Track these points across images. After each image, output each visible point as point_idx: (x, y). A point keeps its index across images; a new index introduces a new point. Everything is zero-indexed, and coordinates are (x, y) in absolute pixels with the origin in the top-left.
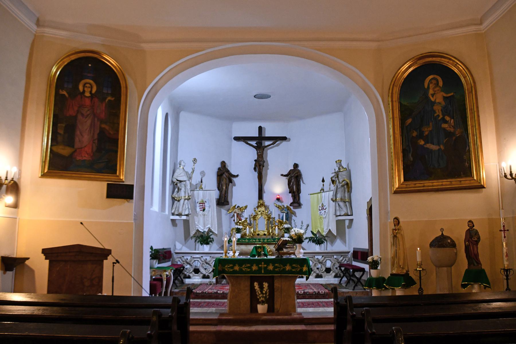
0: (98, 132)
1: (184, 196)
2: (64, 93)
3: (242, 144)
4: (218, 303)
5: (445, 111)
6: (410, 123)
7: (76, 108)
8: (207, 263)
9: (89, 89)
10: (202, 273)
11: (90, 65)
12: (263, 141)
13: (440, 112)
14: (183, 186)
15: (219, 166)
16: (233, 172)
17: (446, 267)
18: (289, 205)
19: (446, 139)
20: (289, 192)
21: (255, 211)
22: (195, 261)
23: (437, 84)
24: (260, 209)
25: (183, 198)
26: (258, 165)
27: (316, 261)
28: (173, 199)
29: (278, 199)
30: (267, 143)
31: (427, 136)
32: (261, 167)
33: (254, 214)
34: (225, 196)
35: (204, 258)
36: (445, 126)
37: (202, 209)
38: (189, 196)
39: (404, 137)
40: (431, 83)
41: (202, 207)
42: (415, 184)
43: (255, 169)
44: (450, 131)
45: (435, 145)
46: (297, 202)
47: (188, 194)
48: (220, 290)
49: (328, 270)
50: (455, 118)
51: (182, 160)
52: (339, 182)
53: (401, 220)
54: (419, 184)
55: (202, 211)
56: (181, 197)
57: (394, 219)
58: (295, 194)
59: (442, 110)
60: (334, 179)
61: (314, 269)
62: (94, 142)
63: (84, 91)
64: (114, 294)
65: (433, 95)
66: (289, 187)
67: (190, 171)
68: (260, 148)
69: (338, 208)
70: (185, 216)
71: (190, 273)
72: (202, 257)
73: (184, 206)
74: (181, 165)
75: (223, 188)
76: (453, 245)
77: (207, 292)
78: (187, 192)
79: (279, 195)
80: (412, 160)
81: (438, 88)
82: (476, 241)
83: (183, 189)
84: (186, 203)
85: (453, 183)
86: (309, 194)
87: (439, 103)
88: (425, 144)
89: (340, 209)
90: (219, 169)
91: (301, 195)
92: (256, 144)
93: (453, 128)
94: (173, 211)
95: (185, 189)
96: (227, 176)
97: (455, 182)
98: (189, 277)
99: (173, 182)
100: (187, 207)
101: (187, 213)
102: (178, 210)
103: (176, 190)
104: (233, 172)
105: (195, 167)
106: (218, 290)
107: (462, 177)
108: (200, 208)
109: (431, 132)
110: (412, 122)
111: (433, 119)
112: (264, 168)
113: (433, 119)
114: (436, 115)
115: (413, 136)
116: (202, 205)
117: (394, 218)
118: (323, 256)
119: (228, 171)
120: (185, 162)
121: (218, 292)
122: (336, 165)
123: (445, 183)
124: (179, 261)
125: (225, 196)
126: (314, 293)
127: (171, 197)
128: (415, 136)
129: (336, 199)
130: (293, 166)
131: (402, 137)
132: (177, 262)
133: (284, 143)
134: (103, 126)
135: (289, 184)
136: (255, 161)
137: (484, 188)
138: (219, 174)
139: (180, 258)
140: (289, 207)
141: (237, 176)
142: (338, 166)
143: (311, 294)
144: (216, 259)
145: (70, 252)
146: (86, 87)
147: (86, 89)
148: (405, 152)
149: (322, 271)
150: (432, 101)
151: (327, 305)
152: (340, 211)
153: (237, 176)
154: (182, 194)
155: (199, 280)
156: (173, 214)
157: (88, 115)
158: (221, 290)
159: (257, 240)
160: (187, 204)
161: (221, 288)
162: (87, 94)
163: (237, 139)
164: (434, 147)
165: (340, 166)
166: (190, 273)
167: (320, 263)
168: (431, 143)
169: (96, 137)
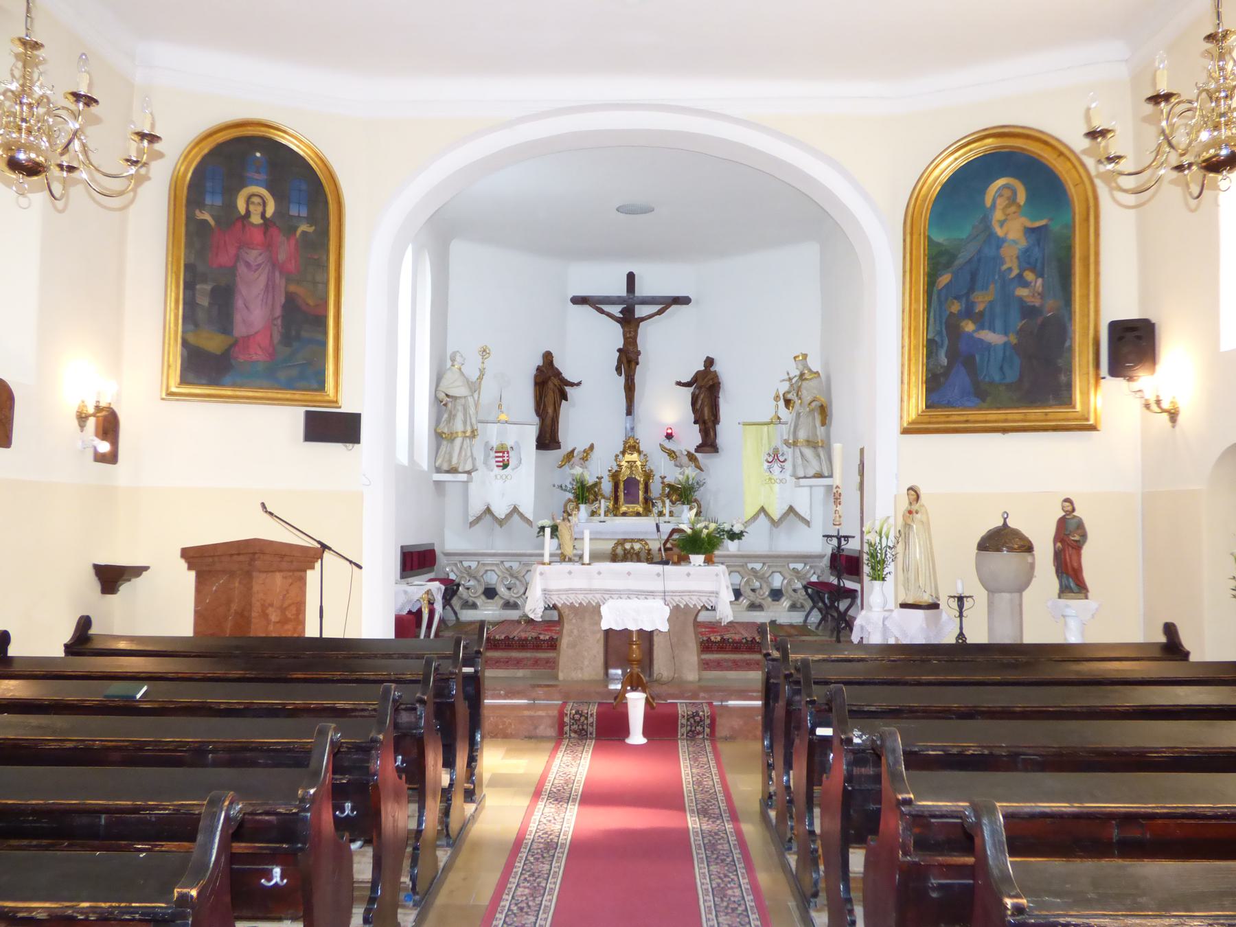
0: (283, 300)
1: (462, 430)
2: (206, 216)
3: (587, 309)
4: (548, 665)
5: (1028, 261)
6: (948, 284)
7: (232, 251)
8: (512, 576)
9: (260, 209)
10: (502, 598)
11: (258, 155)
13: (1015, 261)
14: (460, 408)
15: (539, 361)
18: (693, 451)
19: (1023, 322)
20: (693, 420)
22: (487, 571)
23: (1012, 200)
24: (628, 457)
25: (460, 434)
26: (625, 361)
27: (749, 575)
31: (981, 314)
32: (633, 363)
33: (616, 468)
36: (1022, 292)
37: (501, 464)
39: (932, 314)
40: (1001, 196)
41: (501, 459)
42: (948, 416)
43: (618, 369)
44: (1032, 304)
45: (998, 334)
46: (709, 444)
48: (542, 632)
49: (776, 594)
50: (1046, 276)
51: (458, 352)
53: (922, 492)
54: (957, 415)
55: (501, 468)
56: (457, 433)
57: (908, 490)
58: (707, 426)
59: (1018, 258)
60: (789, 396)
61: (745, 592)
62: (275, 322)
63: (248, 213)
64: (324, 636)
65: (1002, 223)
66: (695, 410)
67: (474, 376)
68: (629, 321)
69: (799, 461)
70: (465, 475)
71: (475, 597)
72: (502, 562)
73: (463, 453)
74: (456, 363)
75: (547, 413)
76: (1028, 548)
77: (516, 638)
78: (468, 423)
79: (671, 429)
80: (946, 364)
81: (1013, 209)
83: (460, 416)
84: (467, 447)
86: (739, 424)
87: (1014, 241)
88: (976, 330)
89: (806, 462)
90: (539, 369)
91: (719, 428)
92: (621, 312)
93: (1039, 297)
96: (556, 385)
98: (474, 606)
101: (468, 468)
102: (450, 461)
103: (446, 416)
104: (568, 375)
105: (485, 366)
106: (540, 634)
107: (1050, 407)
108: (497, 462)
109: (991, 304)
110: (951, 281)
111: (997, 277)
112: (638, 366)
113: (997, 277)
114: (1004, 267)
115: (951, 313)
116: (501, 454)
117: (907, 488)
118: (764, 564)
119: (558, 374)
120: (463, 355)
121: (539, 638)
122: (795, 366)
124: (452, 571)
126: (744, 641)
127: (433, 432)
128: (956, 312)
130: (703, 363)
131: (928, 314)
132: (448, 574)
134: (292, 288)
135: (694, 403)
136: (619, 350)
138: (538, 381)
139: (456, 565)
140: (693, 455)
141: (579, 384)
142: (801, 367)
143: (737, 643)
144: (1006, 263)
145: (239, 554)
146: (253, 203)
147: (252, 208)
148: (931, 347)
149: (762, 596)
150: (998, 238)
151: (748, 666)
152: (805, 467)
153: (579, 384)
155: (497, 612)
156: (439, 470)
157: (259, 265)
158: (546, 633)
160: (469, 448)
161: (546, 628)
162: (256, 219)
163: (579, 300)
164: (992, 337)
165: (805, 367)
166: (475, 597)
167: (757, 578)
168: (990, 329)
169: (278, 312)
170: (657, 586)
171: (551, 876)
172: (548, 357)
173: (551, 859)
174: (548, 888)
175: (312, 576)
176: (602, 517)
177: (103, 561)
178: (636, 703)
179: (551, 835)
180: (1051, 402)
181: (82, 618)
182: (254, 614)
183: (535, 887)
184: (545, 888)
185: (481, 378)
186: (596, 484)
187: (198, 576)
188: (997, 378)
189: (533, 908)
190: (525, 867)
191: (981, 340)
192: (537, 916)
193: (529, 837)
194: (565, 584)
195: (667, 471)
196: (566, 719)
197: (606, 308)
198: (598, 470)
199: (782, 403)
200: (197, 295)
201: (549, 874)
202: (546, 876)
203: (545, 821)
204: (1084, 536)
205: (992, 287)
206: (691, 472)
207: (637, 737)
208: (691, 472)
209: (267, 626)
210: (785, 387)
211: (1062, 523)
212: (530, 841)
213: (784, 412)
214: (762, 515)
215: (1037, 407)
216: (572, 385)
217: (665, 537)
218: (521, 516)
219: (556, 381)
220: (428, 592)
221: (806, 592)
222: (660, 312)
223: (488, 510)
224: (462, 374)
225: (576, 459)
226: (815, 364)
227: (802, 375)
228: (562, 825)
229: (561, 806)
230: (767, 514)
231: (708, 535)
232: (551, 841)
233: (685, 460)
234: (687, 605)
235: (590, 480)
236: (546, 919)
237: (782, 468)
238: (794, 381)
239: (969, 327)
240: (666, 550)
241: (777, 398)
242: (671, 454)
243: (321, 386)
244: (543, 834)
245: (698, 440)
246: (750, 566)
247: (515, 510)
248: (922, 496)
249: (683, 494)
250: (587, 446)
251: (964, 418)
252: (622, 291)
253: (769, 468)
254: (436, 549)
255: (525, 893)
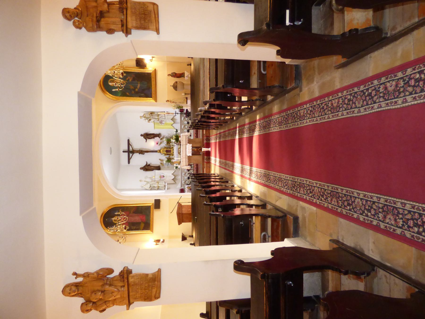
3: (131, 161)
11: (107, 220)
12: (130, 150)
14: (152, 185)
15: (142, 170)
16: (145, 164)
17: (184, 86)
18: (160, 139)
21: (162, 154)
24: (162, 152)
26: (141, 153)
28: (158, 189)
29: (157, 144)
30: (131, 149)
31: (134, 87)
32: (142, 151)
33: (164, 154)
34: (156, 167)
35: (183, 175)
36: (130, 80)
38: (157, 182)
43: (143, 154)
46: (158, 135)
47: (156, 183)
52: (150, 117)
53: (167, 100)
54: (153, 92)
60: (149, 120)
67: (146, 183)
68: (133, 152)
70: (166, 184)
76: (176, 82)
78: (155, 183)
82: (175, 74)
83: (154, 185)
85: (153, 78)
90: (144, 170)
94: (164, 189)
95: (154, 184)
97: (153, 79)
99: (151, 189)
100: (161, 183)
101: (164, 183)
102: (163, 187)
104: (145, 164)
107: (151, 76)
119: (145, 166)
123: (153, 83)
125: (156, 167)
129: (158, 119)
133: (130, 141)
134: (132, 212)
135: (150, 139)
136: (139, 154)
137: (155, 69)
139: (183, 185)
141: (147, 162)
152: (163, 117)
153: (147, 162)
154: (156, 185)
156: (165, 189)
159: (416, 214)
163: (129, 163)
164: (139, 86)
168: (137, 86)
169: (136, 215)
170: (184, 146)
171: (275, 176)
172: (141, 168)
173: (269, 175)
174: (279, 177)
175: (183, 204)
176: (174, 157)
177: (181, 239)
178: (204, 149)
179: (261, 175)
180: (150, 76)
181: (189, 237)
182: (189, 213)
183: (279, 181)
184: (279, 177)
185: (146, 181)
186: (167, 158)
187: (182, 222)
188: (146, 85)
189: (286, 181)
190: (272, 183)
191: (139, 88)
192: (289, 180)
193: (262, 182)
194: (184, 163)
195: (164, 144)
196: (207, 161)
197: (130, 157)
198: (164, 158)
199: (150, 121)
200: (134, 228)
201: (274, 176)
202: (294, 182)
203: (257, 177)
204: (174, 73)
205: (129, 86)
206: (164, 139)
207: (210, 149)
208: (164, 139)
209: (190, 210)
210: (147, 121)
211: (172, 76)
212: (263, 181)
213: (152, 121)
214: (173, 125)
215: (151, 79)
216: (147, 163)
217: (176, 145)
218: (174, 173)
219: (146, 167)
220: (187, 187)
221: (187, 117)
222: (131, 146)
223: (173, 179)
224: (145, 185)
225: (162, 163)
226: (142, 115)
227: (144, 117)
228: (258, 172)
229: (244, 169)
230: (172, 124)
231: (175, 137)
232: (278, 179)
233: (162, 140)
234: (188, 141)
235: (166, 160)
236: (272, 173)
237: (163, 121)
238: (145, 119)
239: (137, 90)
240: (178, 144)
241: (149, 122)
242: (161, 143)
243: (150, 207)
244: (261, 177)
245: (158, 138)
246: (182, 128)
247: (173, 174)
248: (168, 100)
249: (169, 141)
250: (159, 160)
251: (154, 91)
252: (127, 154)
253: (163, 124)
254: (180, 189)
255: (281, 183)
